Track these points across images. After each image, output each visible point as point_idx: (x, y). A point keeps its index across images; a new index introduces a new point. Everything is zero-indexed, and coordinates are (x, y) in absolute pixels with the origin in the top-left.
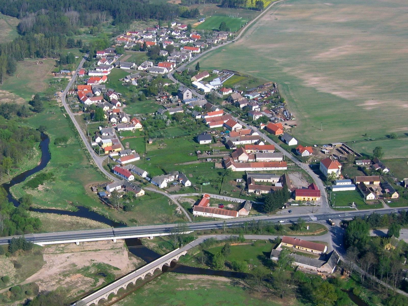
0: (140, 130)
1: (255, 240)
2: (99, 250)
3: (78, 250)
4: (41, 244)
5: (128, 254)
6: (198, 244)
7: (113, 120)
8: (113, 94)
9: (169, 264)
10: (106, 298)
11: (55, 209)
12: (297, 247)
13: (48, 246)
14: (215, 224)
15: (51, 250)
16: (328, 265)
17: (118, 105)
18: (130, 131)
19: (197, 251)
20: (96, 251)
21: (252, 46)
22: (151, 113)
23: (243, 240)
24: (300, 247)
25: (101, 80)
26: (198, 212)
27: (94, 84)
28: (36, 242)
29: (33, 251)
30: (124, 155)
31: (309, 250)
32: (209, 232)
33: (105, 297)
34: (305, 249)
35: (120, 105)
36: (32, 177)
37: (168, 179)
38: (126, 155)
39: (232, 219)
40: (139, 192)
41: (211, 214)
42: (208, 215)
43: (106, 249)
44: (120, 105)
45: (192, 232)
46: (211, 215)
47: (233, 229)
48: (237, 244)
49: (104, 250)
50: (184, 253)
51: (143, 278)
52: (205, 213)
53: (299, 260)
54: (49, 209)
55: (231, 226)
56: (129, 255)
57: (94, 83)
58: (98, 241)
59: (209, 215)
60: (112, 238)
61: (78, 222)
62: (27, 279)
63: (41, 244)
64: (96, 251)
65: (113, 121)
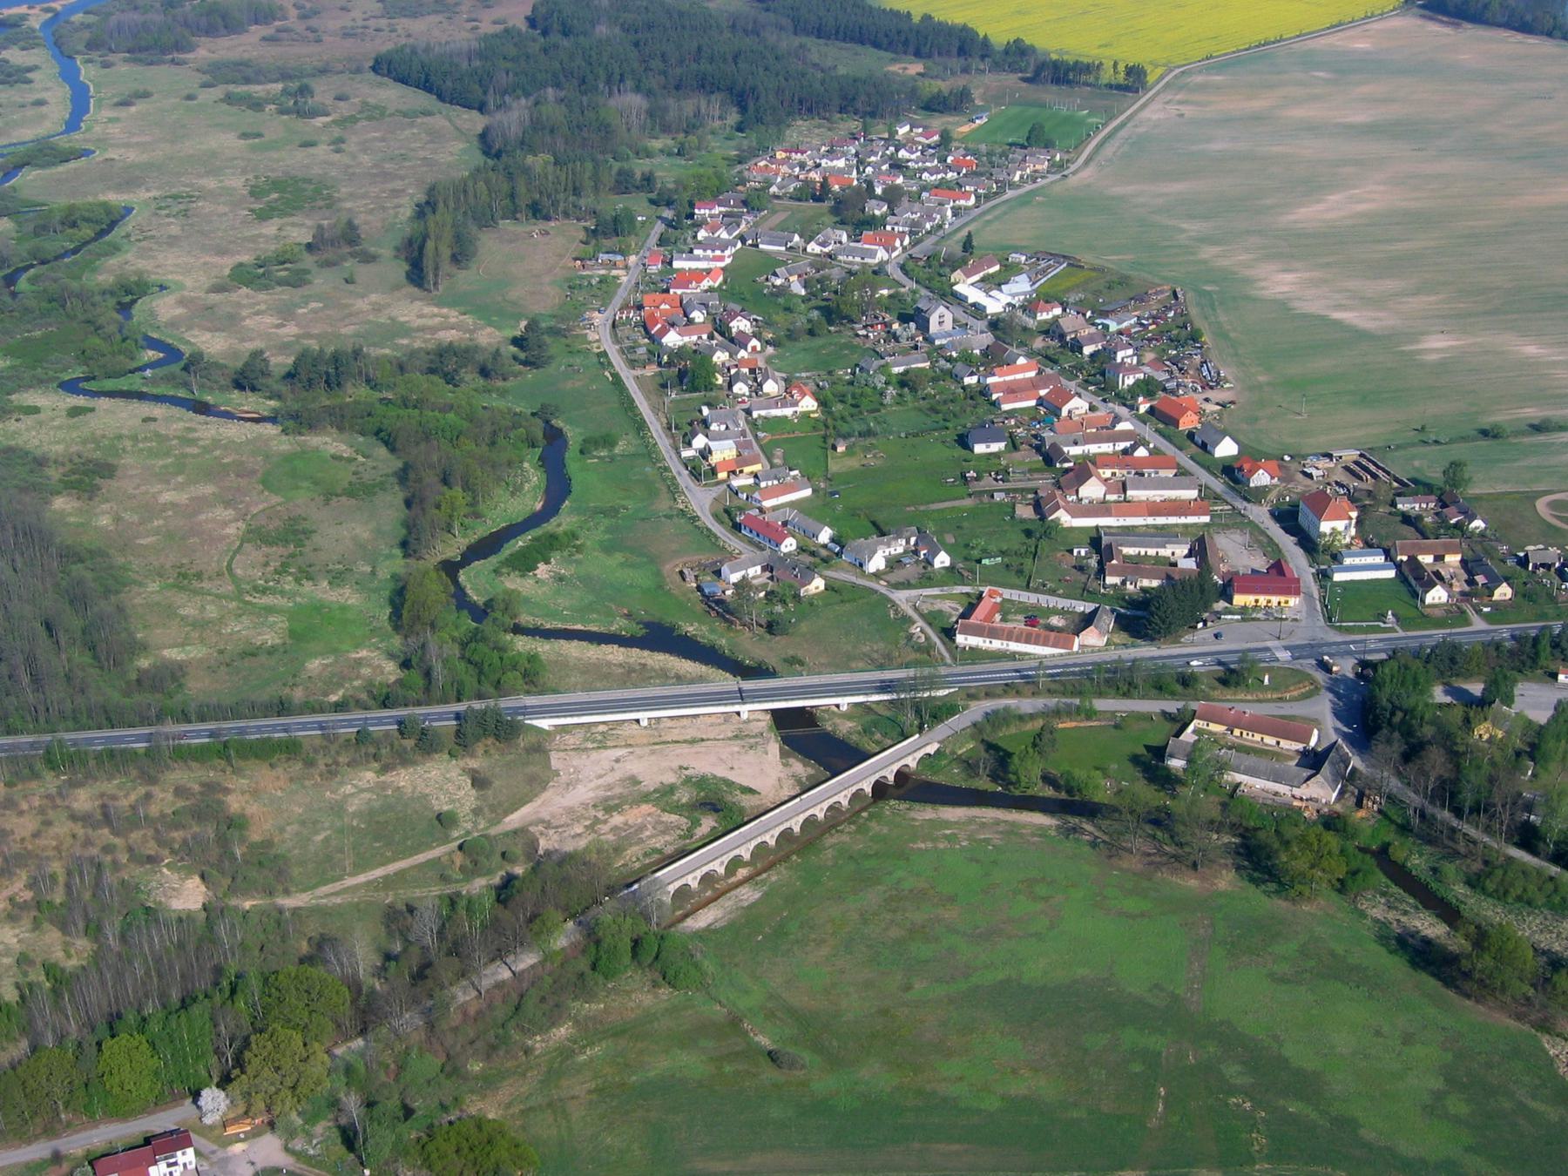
2: (703, 740)
4: (545, 723)
5: (781, 749)
10: (721, 870)
12: (1237, 732)
14: (1017, 671)
15: (571, 740)
17: (754, 348)
20: (693, 742)
23: (1090, 714)
30: (770, 483)
31: (1270, 740)
34: (1258, 737)
35: (759, 349)
36: (520, 543)
38: (776, 482)
39: (1062, 655)
42: (997, 644)
44: (759, 349)
46: (1004, 647)
47: (1062, 683)
48: (1074, 724)
52: (988, 640)
56: (783, 754)
58: (698, 715)
61: (644, 665)
62: (507, 819)
63: (545, 723)
64: (693, 742)
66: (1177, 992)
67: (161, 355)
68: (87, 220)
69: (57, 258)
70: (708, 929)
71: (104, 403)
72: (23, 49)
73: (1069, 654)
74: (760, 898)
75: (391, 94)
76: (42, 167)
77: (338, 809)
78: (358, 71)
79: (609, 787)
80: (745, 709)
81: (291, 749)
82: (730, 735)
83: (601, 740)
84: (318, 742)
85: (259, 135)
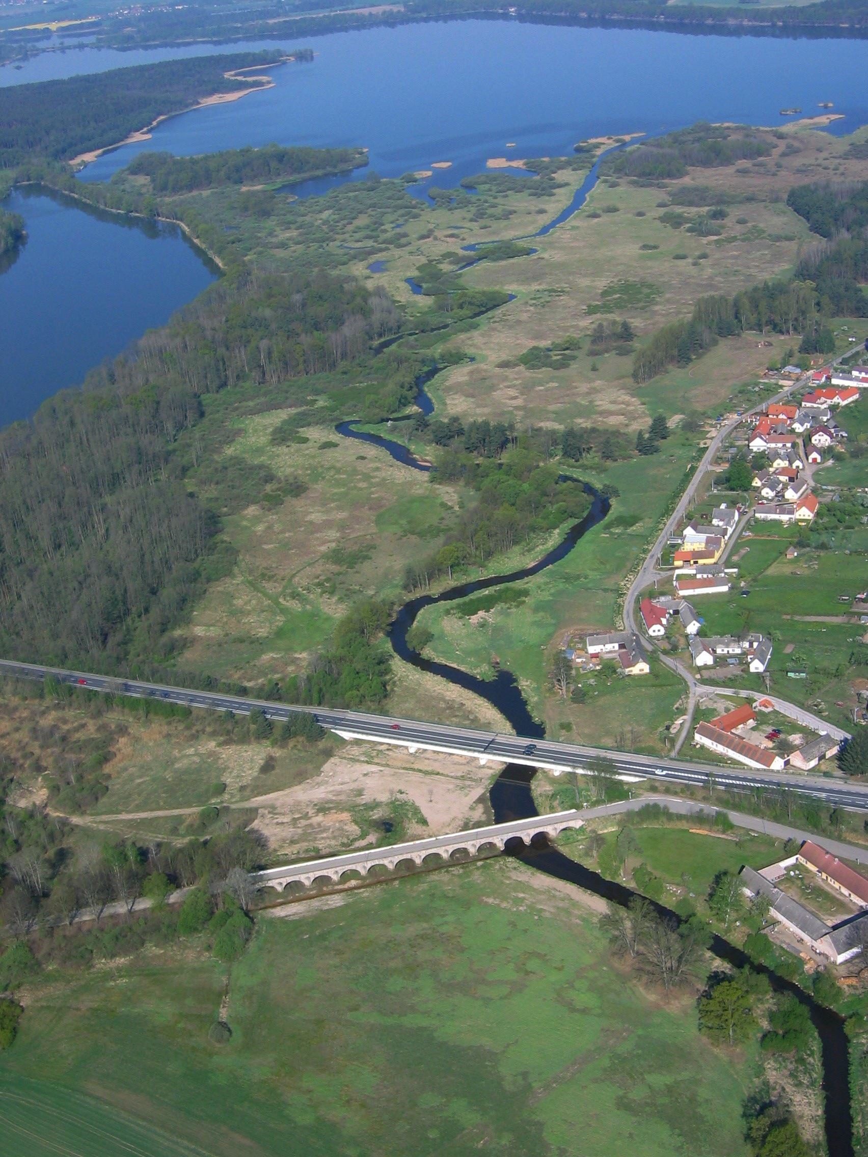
0: (800, 524)
1: (758, 832)
2: (438, 774)
3: (399, 765)
4: (347, 735)
6: (625, 811)
7: (767, 493)
8: (821, 433)
9: (527, 840)
10: (335, 878)
11: (456, 667)
12: (824, 876)
13: (358, 742)
14: (707, 775)
15: (355, 751)
16: (830, 940)
17: (815, 460)
18: (779, 523)
19: (611, 826)
20: (426, 773)
21: (580, 421)
22: (860, 487)
23: (728, 826)
24: (829, 878)
25: (836, 398)
26: (703, 737)
27: (815, 405)
28: (336, 729)
29: (322, 745)
30: (705, 576)
31: (845, 891)
32: (678, 790)
33: (306, 879)
34: (837, 885)
35: (819, 460)
36: (486, 592)
37: (727, 647)
38: (710, 576)
39: (758, 770)
40: (634, 666)
41: (726, 748)
42: (720, 749)
43: (452, 774)
44: (819, 460)
45: (642, 779)
46: (725, 752)
47: (733, 795)
48: (705, 832)
49: (448, 776)
50: (577, 824)
51: (418, 861)
52: (715, 743)
53: (783, 909)
54: (446, 665)
55: (736, 786)
56: (480, 800)
57: (815, 403)
58: (453, 754)
59: (722, 751)
60: (476, 755)
61: (463, 705)
62: (253, 800)
63: (347, 735)
64: (426, 773)
65: (766, 496)
66: (533, 1085)
67: (420, 410)
68: (470, 303)
69: (433, 330)
70: (282, 919)
71: (350, 441)
72: (573, 170)
73: (765, 770)
74: (343, 905)
75: (521, 244)
76: (495, 260)
77: (170, 762)
78: (776, 200)
79: (339, 793)
80: (484, 758)
81: (171, 711)
82: (459, 774)
83: (373, 755)
84: (202, 713)
85: (655, 247)
